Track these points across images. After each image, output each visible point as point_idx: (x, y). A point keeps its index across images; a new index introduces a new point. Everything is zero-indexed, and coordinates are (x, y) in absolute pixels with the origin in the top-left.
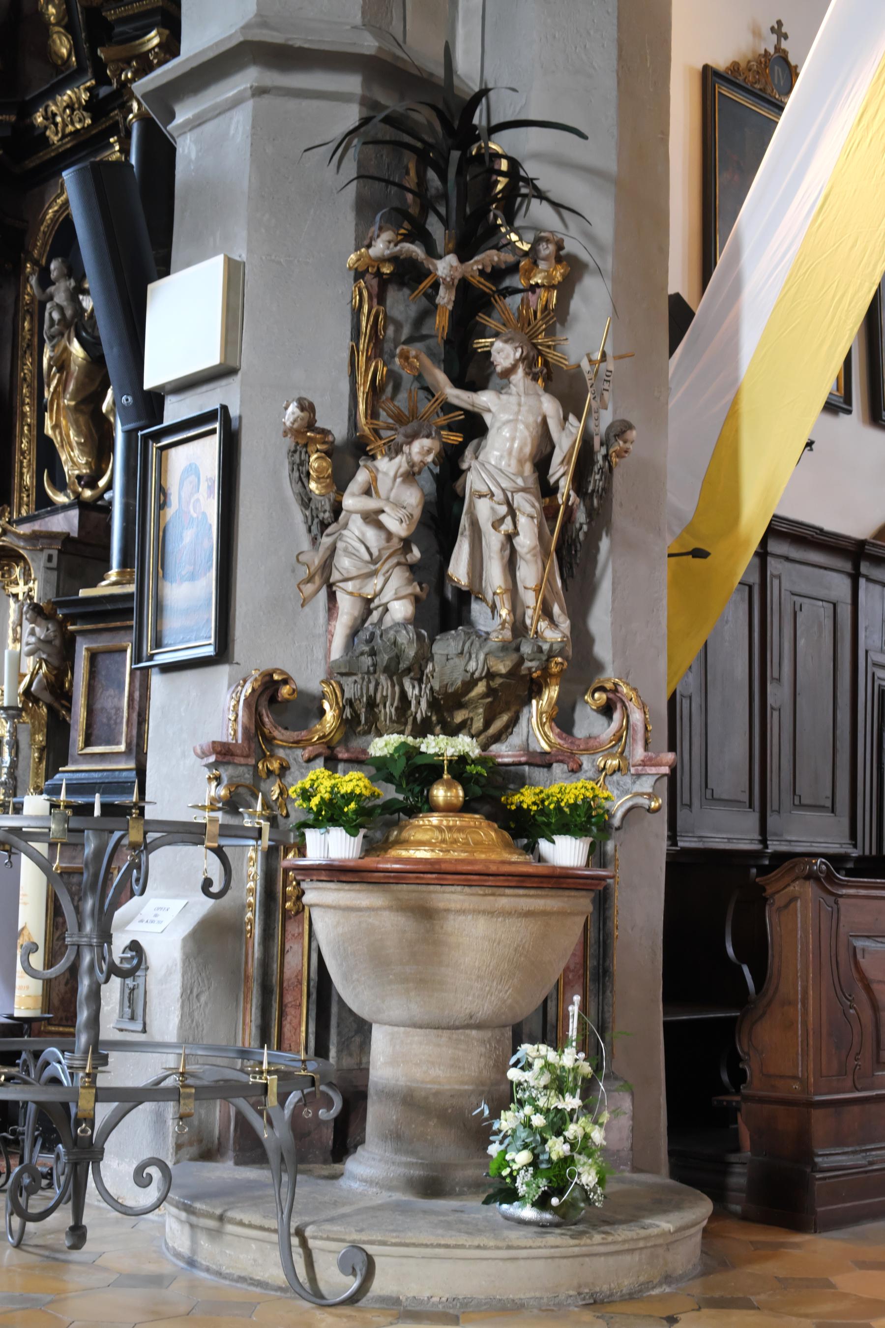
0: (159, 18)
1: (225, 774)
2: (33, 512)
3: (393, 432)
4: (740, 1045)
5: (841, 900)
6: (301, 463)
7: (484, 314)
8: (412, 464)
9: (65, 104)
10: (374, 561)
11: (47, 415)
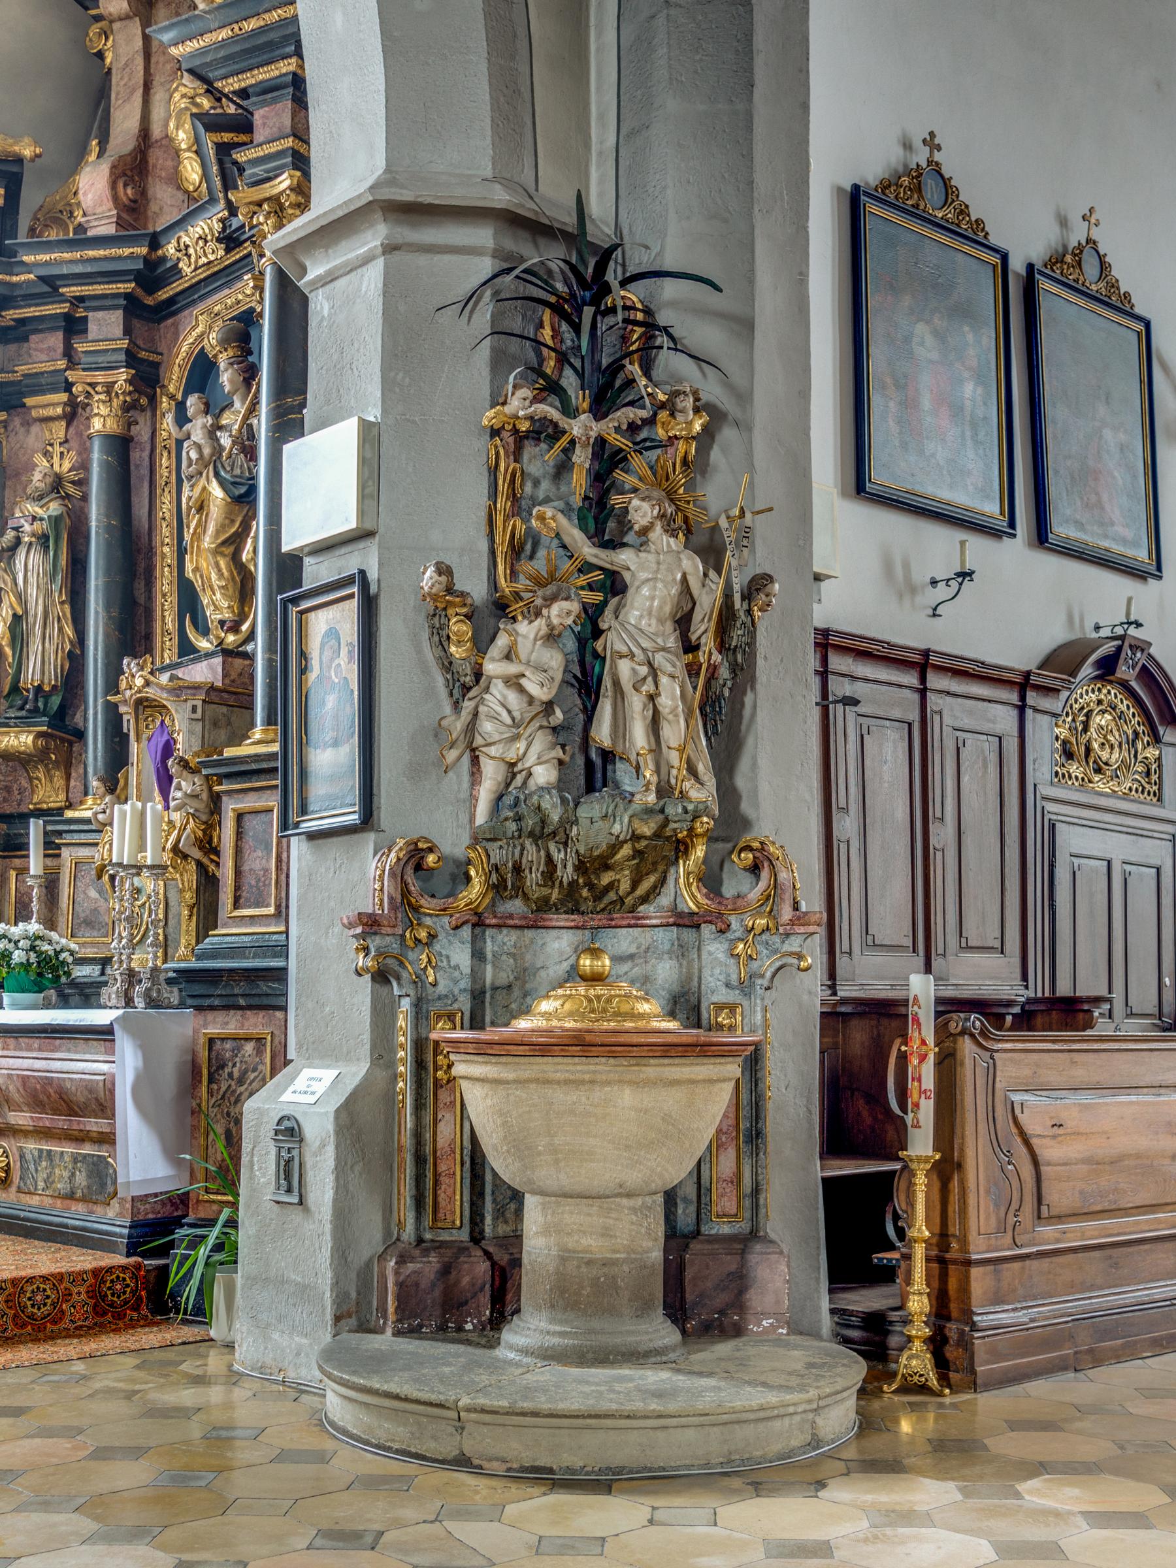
0: (290, 159)
1: (374, 944)
2: (176, 659)
5: (996, 1055)
8: (551, 627)
10: (516, 724)
11: (187, 557)
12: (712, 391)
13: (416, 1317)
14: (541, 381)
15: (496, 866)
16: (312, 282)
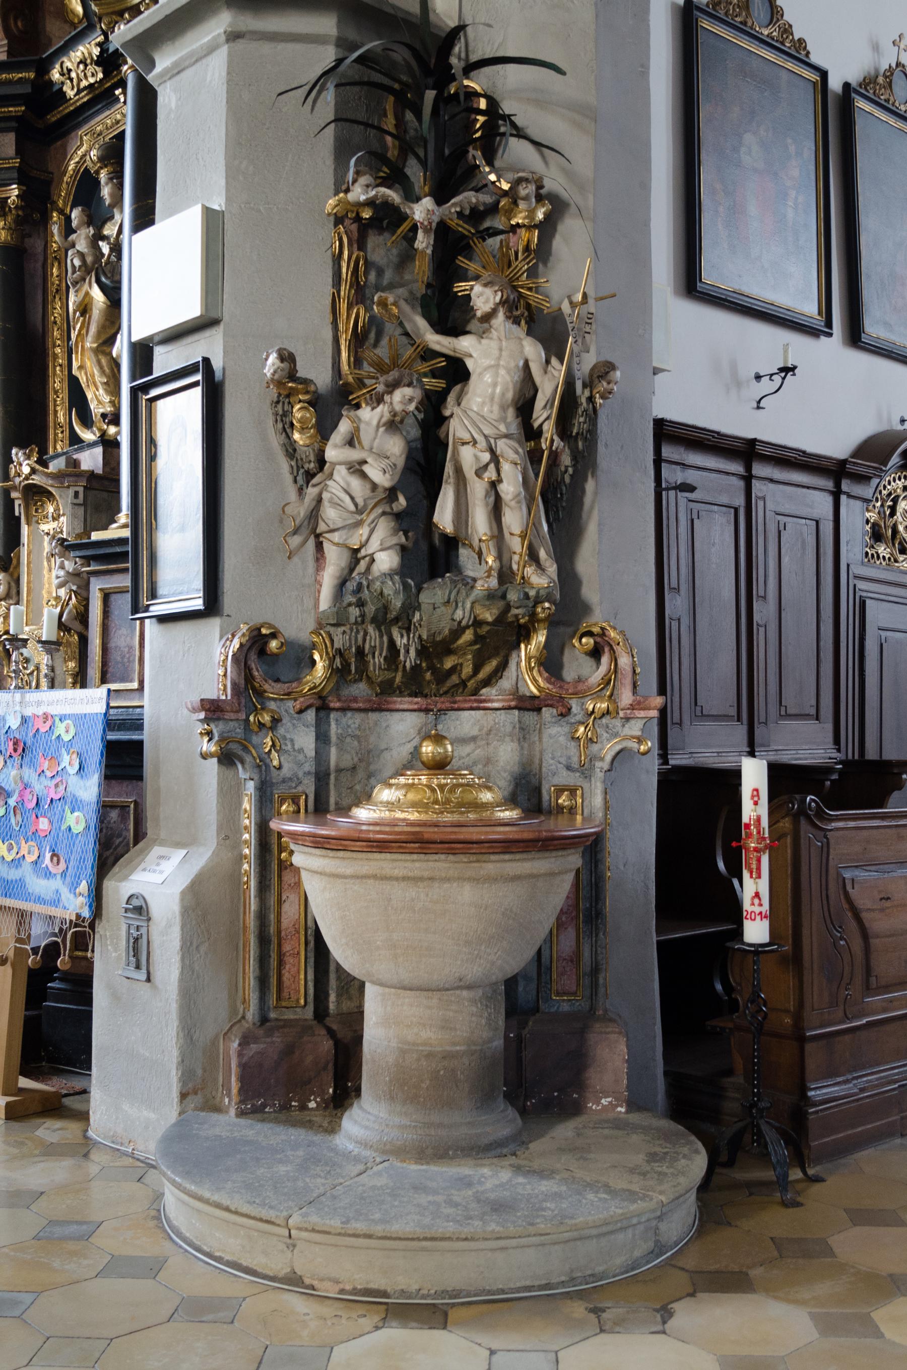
3: (374, 381)
4: (733, 977)
6: (285, 414)
7: (465, 257)
9: (78, 60)
10: (359, 511)
12: (554, 183)
13: (259, 1096)
14: (386, 170)
15: (340, 650)
16: (161, 75)
